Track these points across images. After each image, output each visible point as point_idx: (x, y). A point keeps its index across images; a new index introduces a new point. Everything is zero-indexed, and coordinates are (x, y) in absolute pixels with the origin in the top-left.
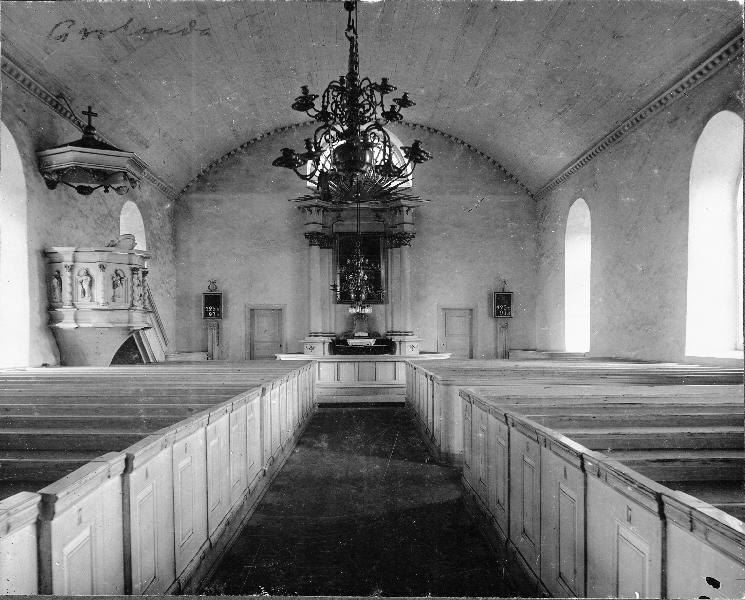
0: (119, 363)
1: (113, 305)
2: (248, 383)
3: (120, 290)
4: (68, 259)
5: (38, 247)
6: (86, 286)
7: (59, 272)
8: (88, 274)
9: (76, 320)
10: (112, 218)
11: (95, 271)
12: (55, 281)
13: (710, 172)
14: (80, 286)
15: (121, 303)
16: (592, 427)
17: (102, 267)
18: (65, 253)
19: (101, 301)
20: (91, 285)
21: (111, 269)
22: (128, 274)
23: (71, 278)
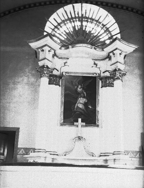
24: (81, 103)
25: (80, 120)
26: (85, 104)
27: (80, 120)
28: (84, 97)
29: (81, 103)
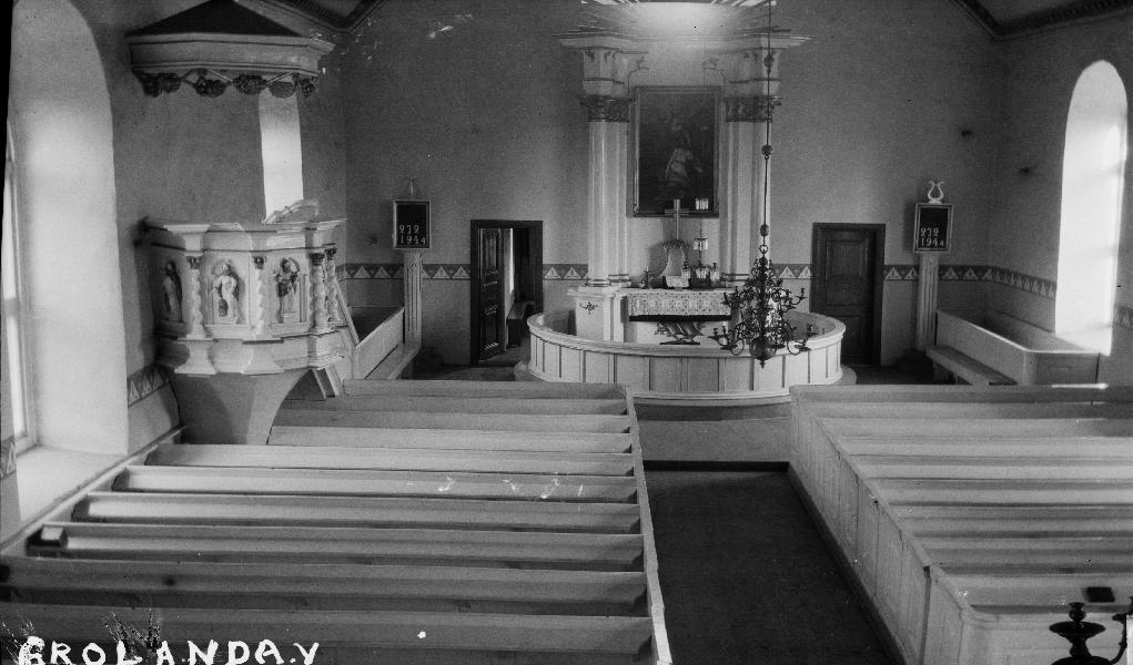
0: (293, 433)
1: (283, 331)
2: (291, 28)
3: (294, 298)
4: (193, 245)
5: (134, 219)
6: (228, 296)
7: (173, 264)
8: (231, 272)
9: (211, 358)
10: (418, 193)
11: (245, 267)
12: (168, 283)
13: (1049, 228)
14: (217, 298)
15: (295, 324)
16: (392, 222)
17: (260, 262)
18: (190, 236)
19: (260, 324)
20: (237, 293)
21: (273, 263)
22: (304, 261)
23: (200, 279)
24: (677, 163)
25: (677, 203)
26: (688, 165)
27: (677, 203)
28: (685, 147)
29: (677, 163)
